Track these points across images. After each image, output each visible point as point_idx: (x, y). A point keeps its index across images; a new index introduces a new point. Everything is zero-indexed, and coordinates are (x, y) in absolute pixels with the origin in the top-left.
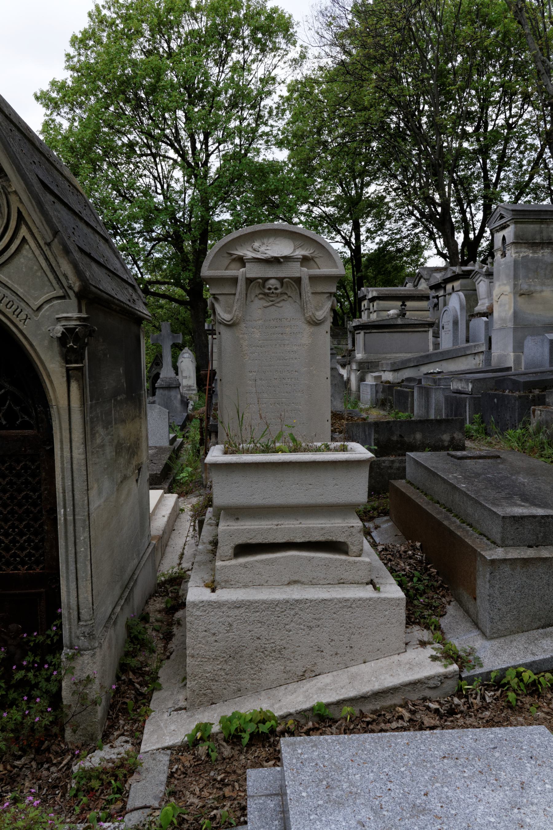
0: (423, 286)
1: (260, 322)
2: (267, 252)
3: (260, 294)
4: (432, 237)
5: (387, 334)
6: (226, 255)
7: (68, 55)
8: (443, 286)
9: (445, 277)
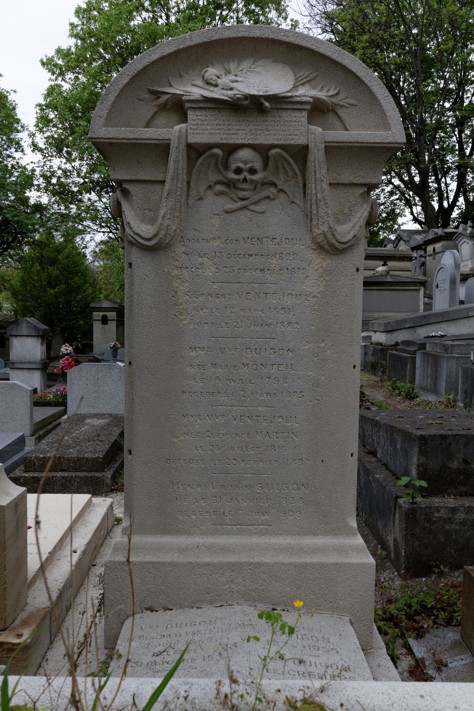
0: (403, 247)
1: (216, 243)
2: (234, 85)
3: (217, 183)
4: (409, 204)
5: (375, 292)
6: (147, 96)
7: (71, 24)
8: (423, 247)
9: (426, 239)
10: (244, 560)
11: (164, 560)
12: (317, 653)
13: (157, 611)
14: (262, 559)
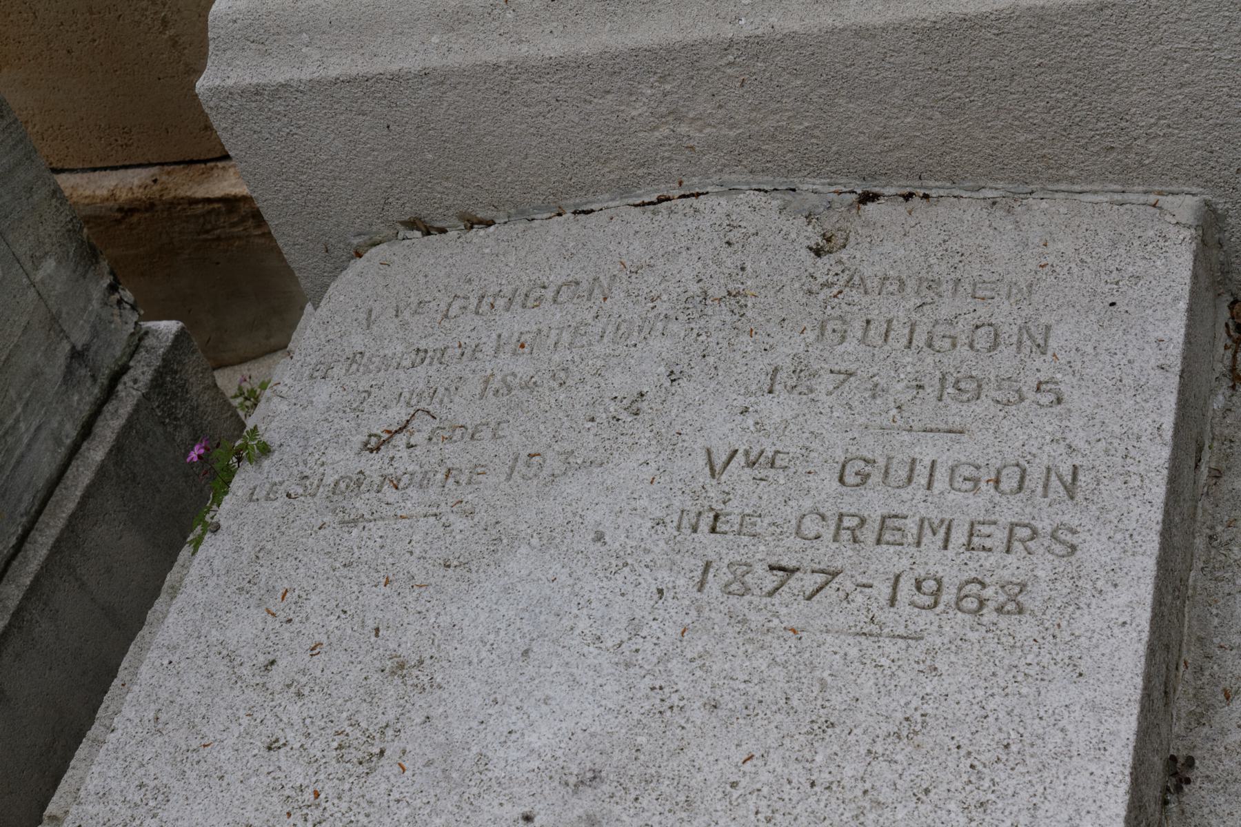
10: (696, 35)
11: (394, 67)
12: (956, 413)
13: (443, 231)
14: (773, 20)
